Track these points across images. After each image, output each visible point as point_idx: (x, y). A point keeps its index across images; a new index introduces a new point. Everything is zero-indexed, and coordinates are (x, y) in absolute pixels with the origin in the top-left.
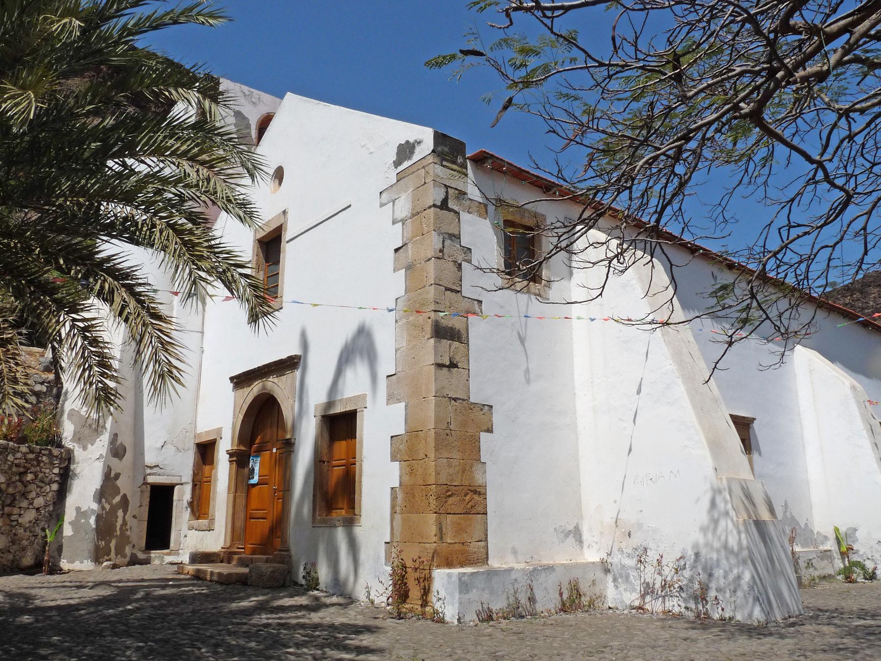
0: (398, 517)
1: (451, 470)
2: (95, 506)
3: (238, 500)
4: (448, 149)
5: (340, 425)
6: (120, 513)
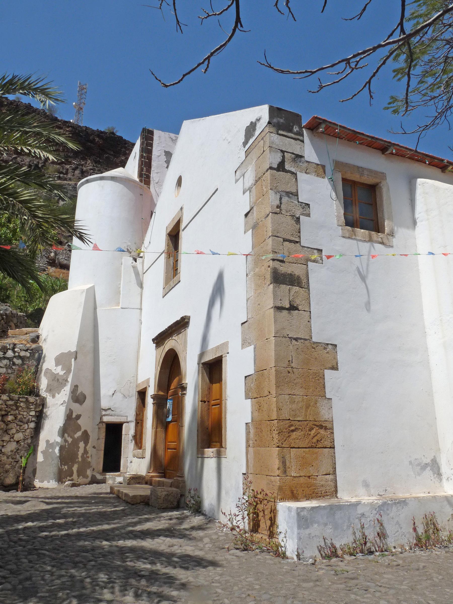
0: (251, 449)
1: (294, 406)
2: (59, 439)
3: (158, 434)
4: (283, 121)
5: (213, 369)
6: (82, 445)
